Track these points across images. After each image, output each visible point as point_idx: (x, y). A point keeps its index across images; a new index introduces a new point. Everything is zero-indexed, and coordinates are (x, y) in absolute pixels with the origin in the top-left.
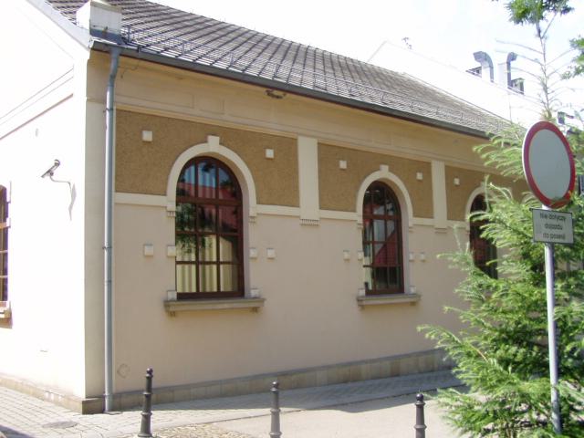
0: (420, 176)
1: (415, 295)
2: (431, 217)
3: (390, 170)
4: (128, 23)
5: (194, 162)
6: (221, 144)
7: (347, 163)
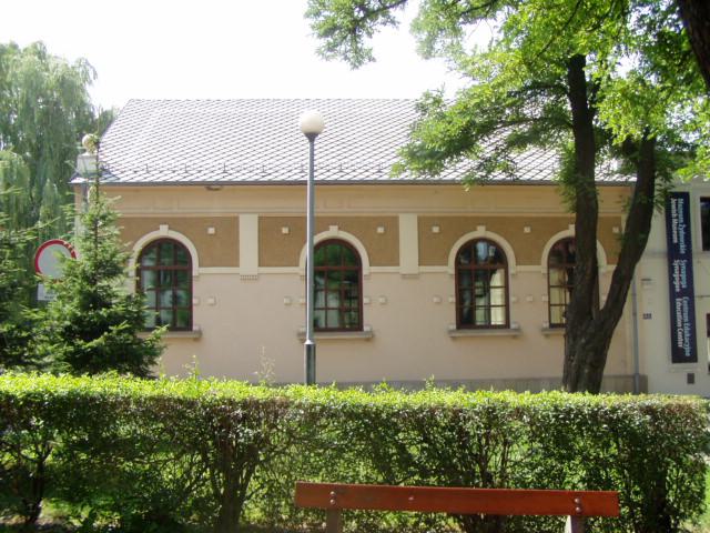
1: (371, 332)
2: (237, 265)
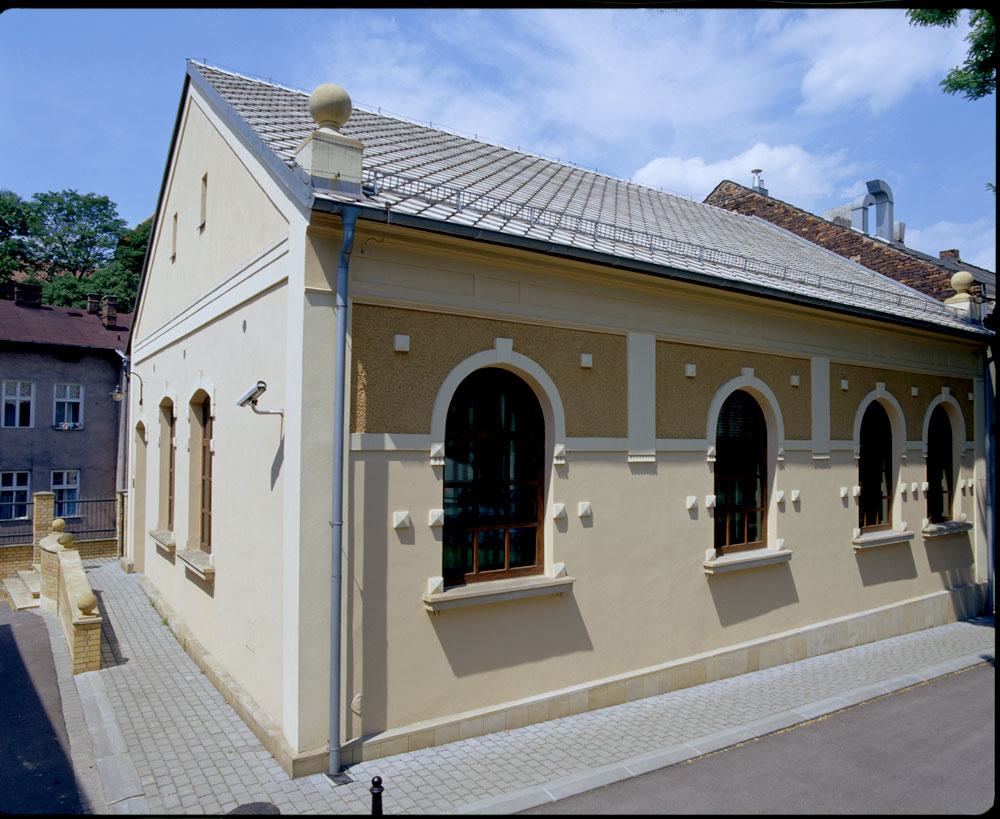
3: (952, 393)
6: (514, 349)
7: (697, 368)
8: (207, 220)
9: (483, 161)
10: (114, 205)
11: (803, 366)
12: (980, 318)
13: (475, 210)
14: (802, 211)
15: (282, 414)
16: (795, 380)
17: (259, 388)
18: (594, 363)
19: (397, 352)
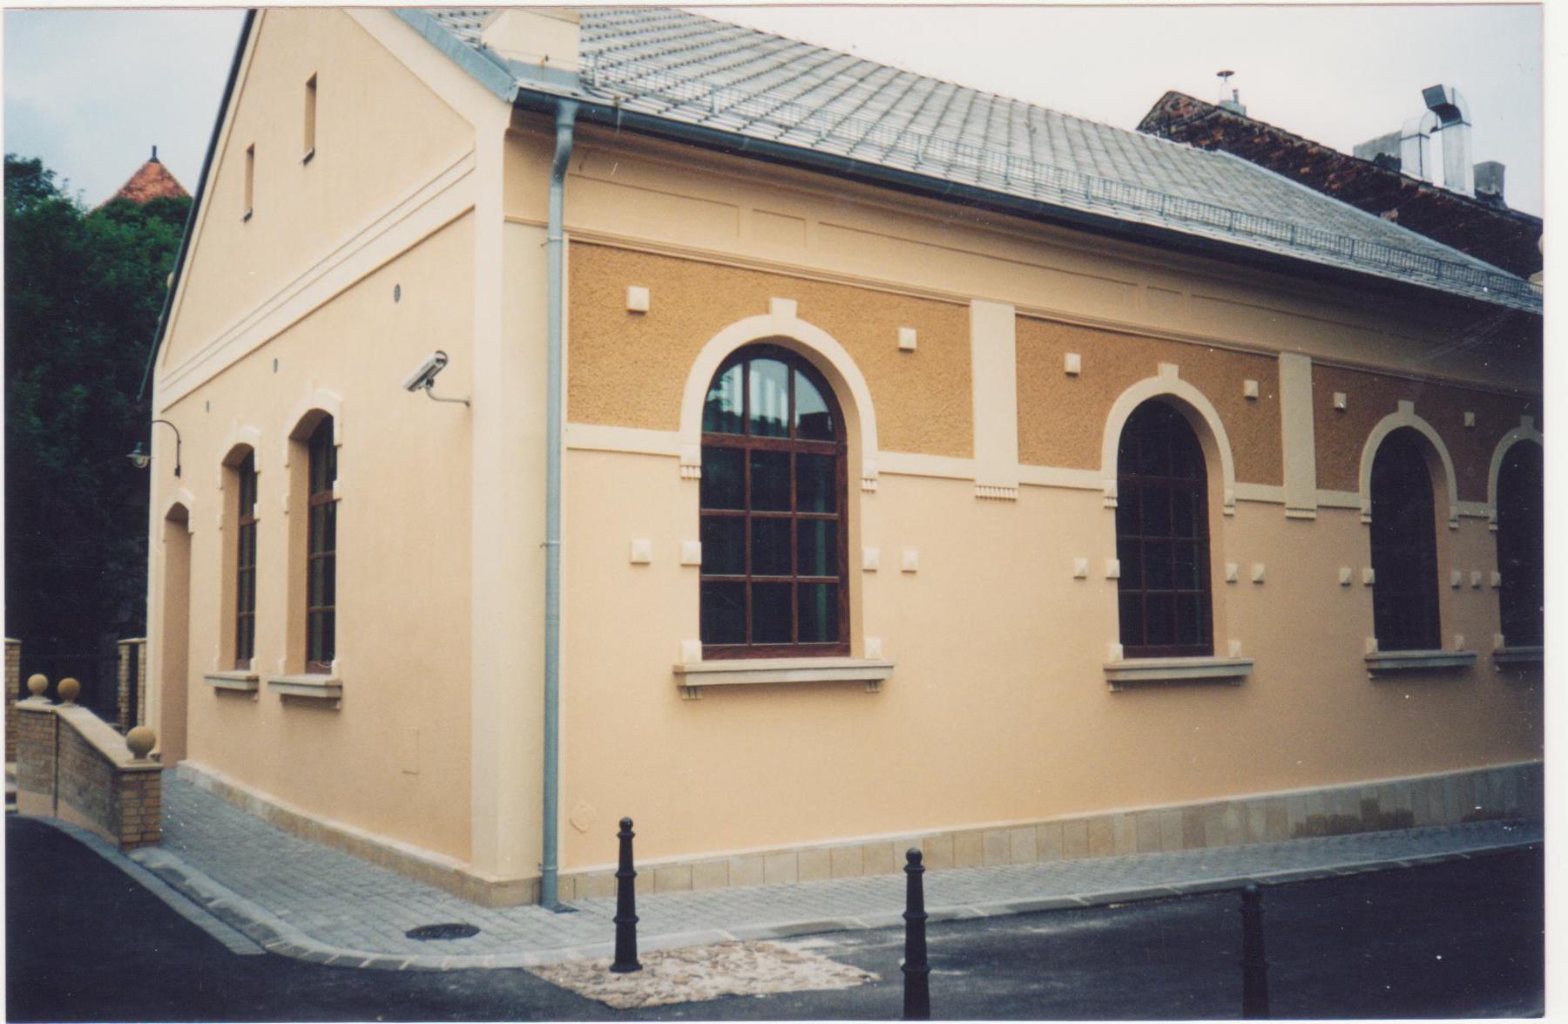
0: (1251, 387)
4: (596, 46)
5: (744, 356)
8: (317, 147)
9: (747, 55)
10: (50, 173)
11: (1265, 363)
12: (1530, 283)
13: (737, 115)
14: (1299, 138)
15: (467, 404)
16: (1251, 387)
17: (438, 360)
18: (918, 342)
19: (633, 312)
